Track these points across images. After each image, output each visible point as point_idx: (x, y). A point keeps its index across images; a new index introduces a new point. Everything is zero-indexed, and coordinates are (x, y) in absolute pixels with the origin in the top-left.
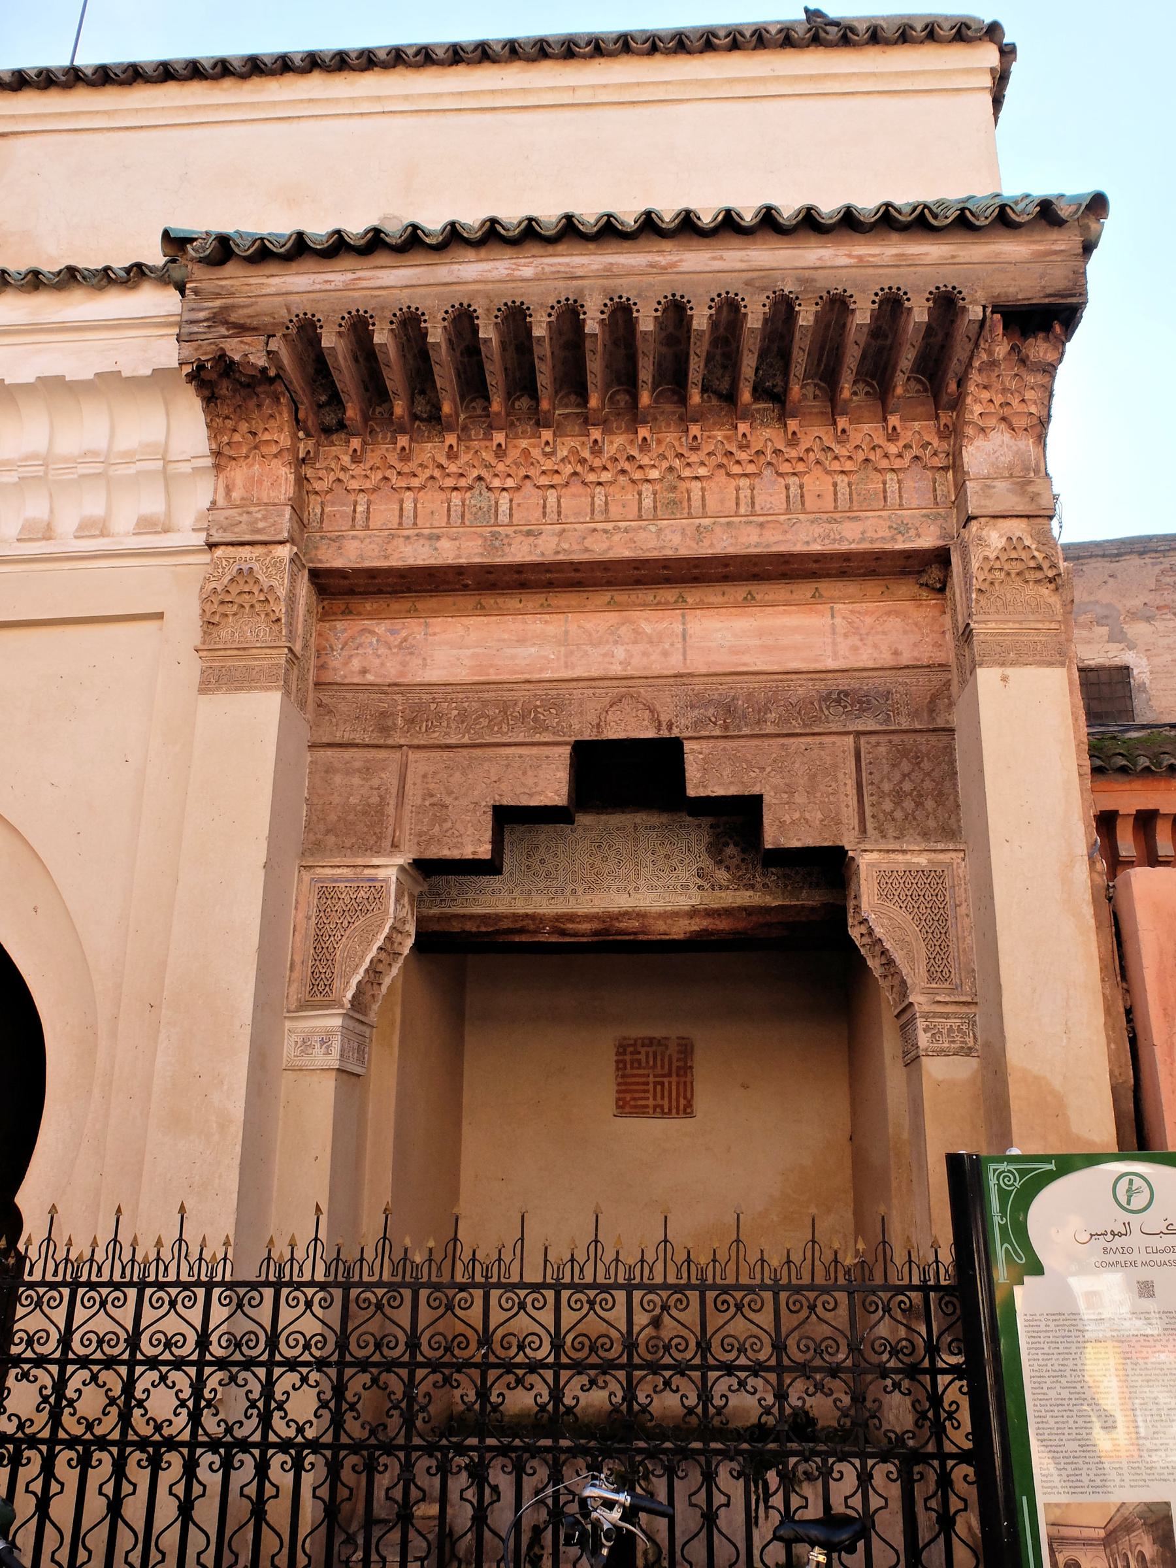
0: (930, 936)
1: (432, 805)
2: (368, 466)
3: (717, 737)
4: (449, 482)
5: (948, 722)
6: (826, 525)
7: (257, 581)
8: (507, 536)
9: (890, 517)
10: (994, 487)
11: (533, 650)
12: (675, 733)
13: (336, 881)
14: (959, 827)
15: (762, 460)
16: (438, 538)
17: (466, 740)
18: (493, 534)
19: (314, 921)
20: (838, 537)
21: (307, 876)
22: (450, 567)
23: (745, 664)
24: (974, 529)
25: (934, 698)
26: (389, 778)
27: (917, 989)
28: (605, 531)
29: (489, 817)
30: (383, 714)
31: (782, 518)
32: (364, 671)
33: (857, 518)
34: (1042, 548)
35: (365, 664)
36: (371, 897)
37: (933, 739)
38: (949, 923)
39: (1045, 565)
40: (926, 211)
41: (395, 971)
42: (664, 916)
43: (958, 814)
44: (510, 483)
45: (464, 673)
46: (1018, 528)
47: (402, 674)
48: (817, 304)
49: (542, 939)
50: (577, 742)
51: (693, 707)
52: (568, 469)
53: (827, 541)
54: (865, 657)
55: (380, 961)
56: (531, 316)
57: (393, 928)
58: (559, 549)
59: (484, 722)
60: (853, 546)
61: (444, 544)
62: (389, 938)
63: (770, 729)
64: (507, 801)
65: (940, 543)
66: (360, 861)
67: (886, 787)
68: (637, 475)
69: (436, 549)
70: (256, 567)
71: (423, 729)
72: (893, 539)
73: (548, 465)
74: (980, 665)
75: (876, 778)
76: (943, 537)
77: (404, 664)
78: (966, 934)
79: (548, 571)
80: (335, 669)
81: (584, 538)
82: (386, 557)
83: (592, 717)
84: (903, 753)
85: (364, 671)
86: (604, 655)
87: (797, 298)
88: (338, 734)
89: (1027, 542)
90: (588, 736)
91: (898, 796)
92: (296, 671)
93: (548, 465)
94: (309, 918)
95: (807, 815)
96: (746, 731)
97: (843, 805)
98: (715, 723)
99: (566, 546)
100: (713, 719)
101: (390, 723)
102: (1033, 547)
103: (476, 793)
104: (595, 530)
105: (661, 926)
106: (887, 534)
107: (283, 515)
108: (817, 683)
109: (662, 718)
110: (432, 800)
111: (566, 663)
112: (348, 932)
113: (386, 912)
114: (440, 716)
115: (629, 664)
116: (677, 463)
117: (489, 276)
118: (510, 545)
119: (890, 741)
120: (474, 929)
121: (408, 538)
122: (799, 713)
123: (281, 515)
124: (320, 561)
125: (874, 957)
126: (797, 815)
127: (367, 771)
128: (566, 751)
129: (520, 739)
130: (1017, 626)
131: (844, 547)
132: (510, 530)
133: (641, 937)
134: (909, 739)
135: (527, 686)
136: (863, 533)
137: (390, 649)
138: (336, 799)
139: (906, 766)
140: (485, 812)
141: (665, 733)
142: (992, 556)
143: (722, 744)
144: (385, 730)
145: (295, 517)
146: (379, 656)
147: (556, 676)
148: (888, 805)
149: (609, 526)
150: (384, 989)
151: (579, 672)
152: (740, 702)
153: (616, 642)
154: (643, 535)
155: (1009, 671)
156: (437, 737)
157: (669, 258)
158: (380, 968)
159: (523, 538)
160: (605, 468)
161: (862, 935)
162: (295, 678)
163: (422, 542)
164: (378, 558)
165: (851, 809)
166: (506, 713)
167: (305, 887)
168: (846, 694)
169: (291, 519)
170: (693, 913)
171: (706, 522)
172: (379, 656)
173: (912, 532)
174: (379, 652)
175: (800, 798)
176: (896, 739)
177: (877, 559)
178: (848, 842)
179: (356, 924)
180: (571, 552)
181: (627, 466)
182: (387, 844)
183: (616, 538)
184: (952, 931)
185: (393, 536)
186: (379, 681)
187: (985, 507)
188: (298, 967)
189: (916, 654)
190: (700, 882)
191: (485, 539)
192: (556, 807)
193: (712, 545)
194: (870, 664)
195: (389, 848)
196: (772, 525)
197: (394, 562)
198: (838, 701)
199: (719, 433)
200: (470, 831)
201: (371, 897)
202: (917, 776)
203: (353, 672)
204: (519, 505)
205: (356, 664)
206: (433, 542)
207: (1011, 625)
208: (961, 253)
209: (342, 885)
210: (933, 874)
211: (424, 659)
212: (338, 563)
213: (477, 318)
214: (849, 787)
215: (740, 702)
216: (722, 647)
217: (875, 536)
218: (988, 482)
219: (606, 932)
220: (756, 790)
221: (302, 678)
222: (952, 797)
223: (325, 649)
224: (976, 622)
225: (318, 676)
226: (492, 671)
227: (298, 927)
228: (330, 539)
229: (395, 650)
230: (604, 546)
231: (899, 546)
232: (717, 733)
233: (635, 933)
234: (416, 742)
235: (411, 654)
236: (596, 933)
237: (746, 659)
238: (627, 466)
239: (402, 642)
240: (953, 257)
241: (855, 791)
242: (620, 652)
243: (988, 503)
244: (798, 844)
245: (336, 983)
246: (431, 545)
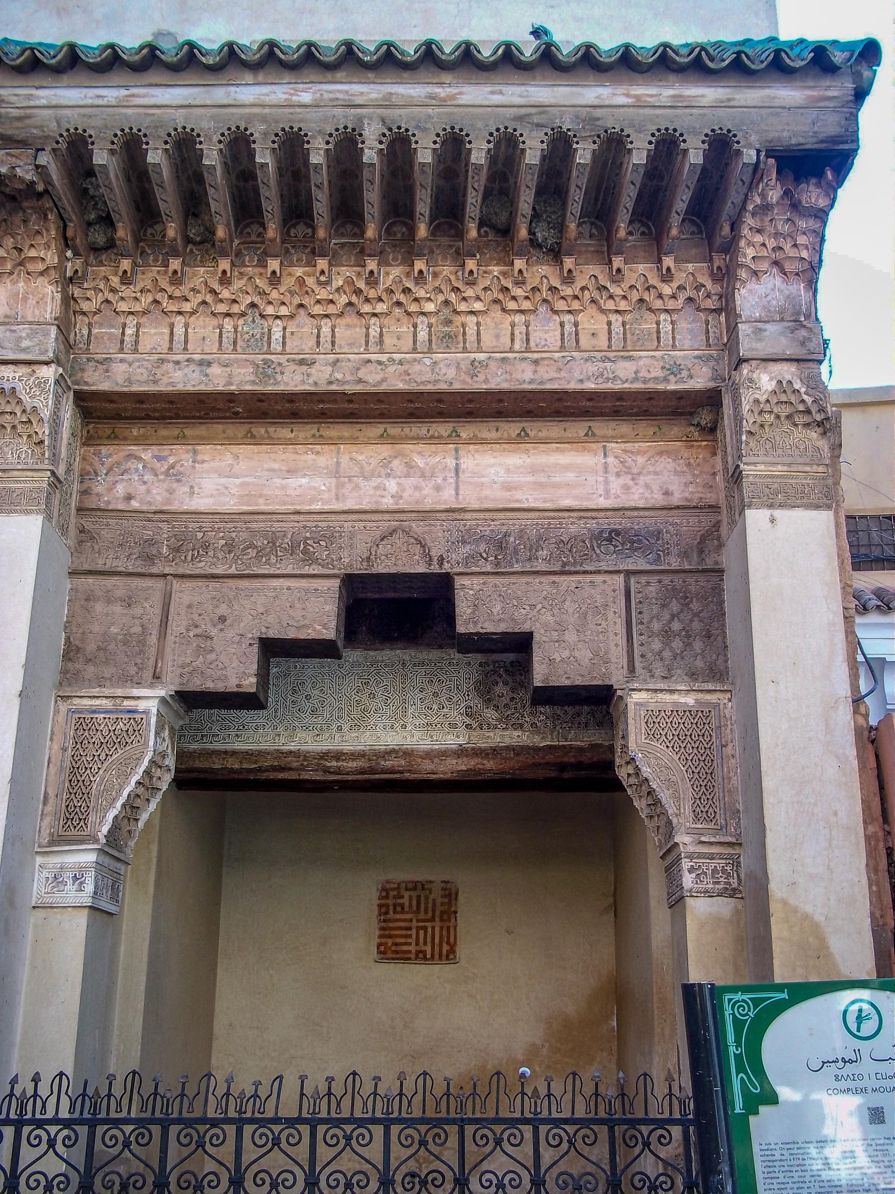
0: (696, 776)
1: (196, 636)
2: (138, 289)
4: (222, 308)
5: (717, 563)
6: (600, 364)
7: (20, 402)
8: (280, 364)
9: (663, 358)
10: (765, 330)
11: (304, 481)
12: (447, 568)
13: (94, 712)
14: (727, 667)
15: (538, 297)
16: (209, 364)
17: (233, 571)
18: (265, 362)
19: (69, 752)
20: (611, 376)
21: (63, 707)
22: (221, 394)
23: (518, 501)
24: (745, 372)
25: (703, 539)
26: (152, 610)
27: (683, 829)
28: (379, 363)
29: (255, 649)
30: (151, 542)
31: (557, 355)
32: (129, 498)
34: (811, 392)
35: (131, 490)
36: (131, 730)
37: (702, 579)
38: (715, 763)
39: (814, 410)
40: (703, 53)
41: (153, 806)
42: (429, 755)
43: (725, 655)
44: (284, 311)
45: (232, 502)
46: (788, 371)
47: (168, 502)
48: (594, 142)
49: (307, 777)
51: (464, 542)
52: (343, 299)
54: (636, 497)
55: (138, 796)
56: (308, 143)
57: (152, 762)
58: (333, 379)
59: (252, 553)
60: (626, 385)
61: (215, 370)
62: (147, 772)
63: (541, 566)
64: (272, 634)
65: (712, 385)
66: (119, 692)
67: (656, 626)
68: (413, 308)
69: (207, 375)
70: (19, 386)
71: (189, 558)
72: (666, 380)
73: (323, 294)
74: (749, 507)
75: (646, 618)
76: (714, 379)
77: (171, 492)
78: (732, 774)
79: (321, 401)
80: (98, 495)
81: (358, 369)
82: (155, 382)
83: (361, 549)
84: (673, 592)
85: (129, 498)
86: (376, 488)
87: (575, 136)
88: (101, 562)
89: (797, 385)
90: (359, 569)
91: (667, 634)
92: (58, 495)
93: (323, 294)
94: (64, 749)
95: (577, 654)
96: (517, 567)
97: (612, 644)
98: (486, 559)
99: (339, 376)
100: (485, 555)
101: (154, 552)
102: (803, 390)
103: (242, 625)
104: (369, 361)
105: (427, 765)
106: (659, 374)
107: (48, 334)
108: (590, 521)
109: (433, 553)
110: (199, 631)
111: (337, 495)
112: (105, 765)
113: (146, 744)
114: (206, 546)
115: (401, 497)
116: (453, 297)
118: (282, 373)
119: (660, 582)
120: (236, 766)
121: (177, 363)
122: (570, 551)
123: (47, 334)
124: (86, 383)
125: (640, 797)
126: (566, 654)
127: (129, 601)
128: (336, 583)
129: (289, 570)
131: (618, 386)
132: (283, 359)
133: (407, 775)
134: (678, 580)
135: (296, 517)
136: (636, 372)
137: (156, 475)
138: (96, 628)
139: (675, 606)
140: (250, 645)
141: (435, 569)
142: (763, 399)
144: (150, 559)
145: (61, 338)
146: (145, 483)
147: (327, 507)
148: (657, 645)
149: (384, 358)
150: (141, 824)
151: (350, 505)
152: (512, 539)
153: (388, 475)
154: (417, 367)
155: (777, 513)
156: (203, 567)
157: (448, 90)
158: (138, 803)
159: (296, 367)
160: (380, 299)
161: (629, 775)
162: (57, 502)
163: (192, 367)
164: (146, 382)
165: (620, 648)
166: (274, 544)
167: (61, 718)
168: (618, 533)
169: (57, 339)
170: (461, 752)
171: (481, 356)
172: (145, 483)
173: (685, 373)
174: (146, 478)
175: (571, 637)
176: (666, 579)
177: (650, 399)
178: (617, 678)
179: (114, 757)
180: (345, 383)
181: (402, 298)
182: (148, 674)
183: (391, 369)
184: (718, 772)
185: (163, 361)
186: (145, 508)
187: (756, 350)
188: (51, 801)
189: (687, 495)
190: (468, 721)
193: (486, 381)
194: (641, 504)
195: (150, 680)
196: (546, 362)
197: (162, 387)
198: (610, 540)
199: (496, 268)
200: (235, 663)
201: (131, 730)
202: (686, 616)
203: (118, 499)
204: (292, 333)
205: (121, 489)
206: (204, 368)
207: (780, 468)
208: (737, 97)
210: (700, 714)
211: (192, 487)
212: (105, 386)
213: (254, 142)
214: (618, 626)
215: (512, 539)
216: (495, 483)
217: (648, 376)
218: (760, 325)
219: (372, 771)
220: (526, 627)
221: (64, 503)
222: (720, 638)
223: (88, 473)
224: (745, 464)
225: (81, 501)
226: (261, 501)
227: (53, 760)
228: (97, 362)
229: (161, 477)
230: (378, 377)
231: (671, 387)
232: (489, 568)
233: (401, 772)
234: (181, 571)
235: (179, 481)
236: (362, 772)
237: (519, 495)
238: (402, 298)
239: (168, 469)
240: (729, 100)
241: (624, 630)
242: (392, 485)
243: (759, 346)
244: (567, 683)
245: (92, 818)
246: (201, 371)
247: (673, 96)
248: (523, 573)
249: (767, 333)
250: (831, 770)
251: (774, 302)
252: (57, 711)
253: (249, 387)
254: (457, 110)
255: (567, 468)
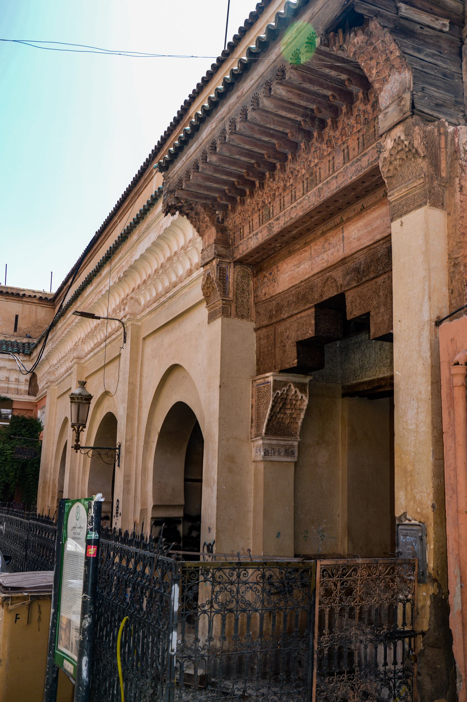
3: (356, 287)
9: (376, 146)
10: (388, 112)
23: (362, 245)
33: (365, 154)
49: (387, 389)
50: (315, 305)
53: (357, 173)
64: (300, 339)
94: (256, 401)
104: (292, 208)
117: (208, 133)
130: (406, 189)
143: (359, 289)
188: (254, 421)
191: (267, 227)
192: (312, 337)
207: (404, 190)
208: (315, 10)
209: (262, 386)
240: (313, 14)
242: (325, 256)
247: (296, 31)
248: (367, 281)
249: (389, 113)
250: (420, 368)
251: (395, 90)
252: (253, 387)
253: (267, 238)
254: (247, 94)
255: (377, 218)
